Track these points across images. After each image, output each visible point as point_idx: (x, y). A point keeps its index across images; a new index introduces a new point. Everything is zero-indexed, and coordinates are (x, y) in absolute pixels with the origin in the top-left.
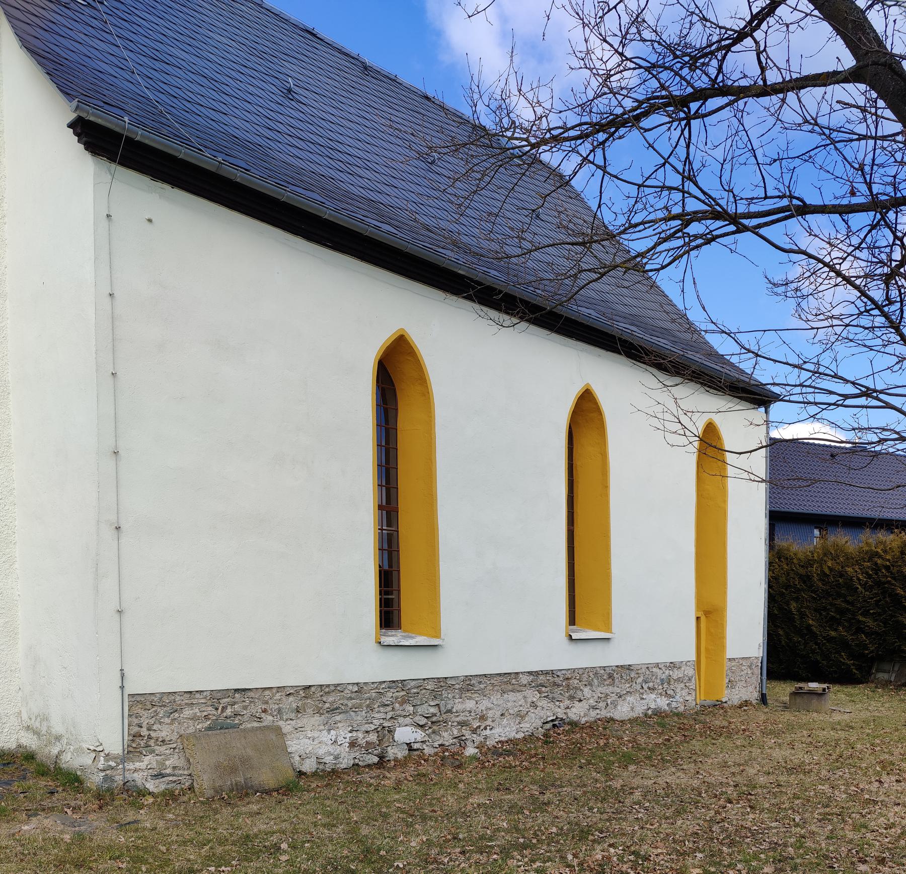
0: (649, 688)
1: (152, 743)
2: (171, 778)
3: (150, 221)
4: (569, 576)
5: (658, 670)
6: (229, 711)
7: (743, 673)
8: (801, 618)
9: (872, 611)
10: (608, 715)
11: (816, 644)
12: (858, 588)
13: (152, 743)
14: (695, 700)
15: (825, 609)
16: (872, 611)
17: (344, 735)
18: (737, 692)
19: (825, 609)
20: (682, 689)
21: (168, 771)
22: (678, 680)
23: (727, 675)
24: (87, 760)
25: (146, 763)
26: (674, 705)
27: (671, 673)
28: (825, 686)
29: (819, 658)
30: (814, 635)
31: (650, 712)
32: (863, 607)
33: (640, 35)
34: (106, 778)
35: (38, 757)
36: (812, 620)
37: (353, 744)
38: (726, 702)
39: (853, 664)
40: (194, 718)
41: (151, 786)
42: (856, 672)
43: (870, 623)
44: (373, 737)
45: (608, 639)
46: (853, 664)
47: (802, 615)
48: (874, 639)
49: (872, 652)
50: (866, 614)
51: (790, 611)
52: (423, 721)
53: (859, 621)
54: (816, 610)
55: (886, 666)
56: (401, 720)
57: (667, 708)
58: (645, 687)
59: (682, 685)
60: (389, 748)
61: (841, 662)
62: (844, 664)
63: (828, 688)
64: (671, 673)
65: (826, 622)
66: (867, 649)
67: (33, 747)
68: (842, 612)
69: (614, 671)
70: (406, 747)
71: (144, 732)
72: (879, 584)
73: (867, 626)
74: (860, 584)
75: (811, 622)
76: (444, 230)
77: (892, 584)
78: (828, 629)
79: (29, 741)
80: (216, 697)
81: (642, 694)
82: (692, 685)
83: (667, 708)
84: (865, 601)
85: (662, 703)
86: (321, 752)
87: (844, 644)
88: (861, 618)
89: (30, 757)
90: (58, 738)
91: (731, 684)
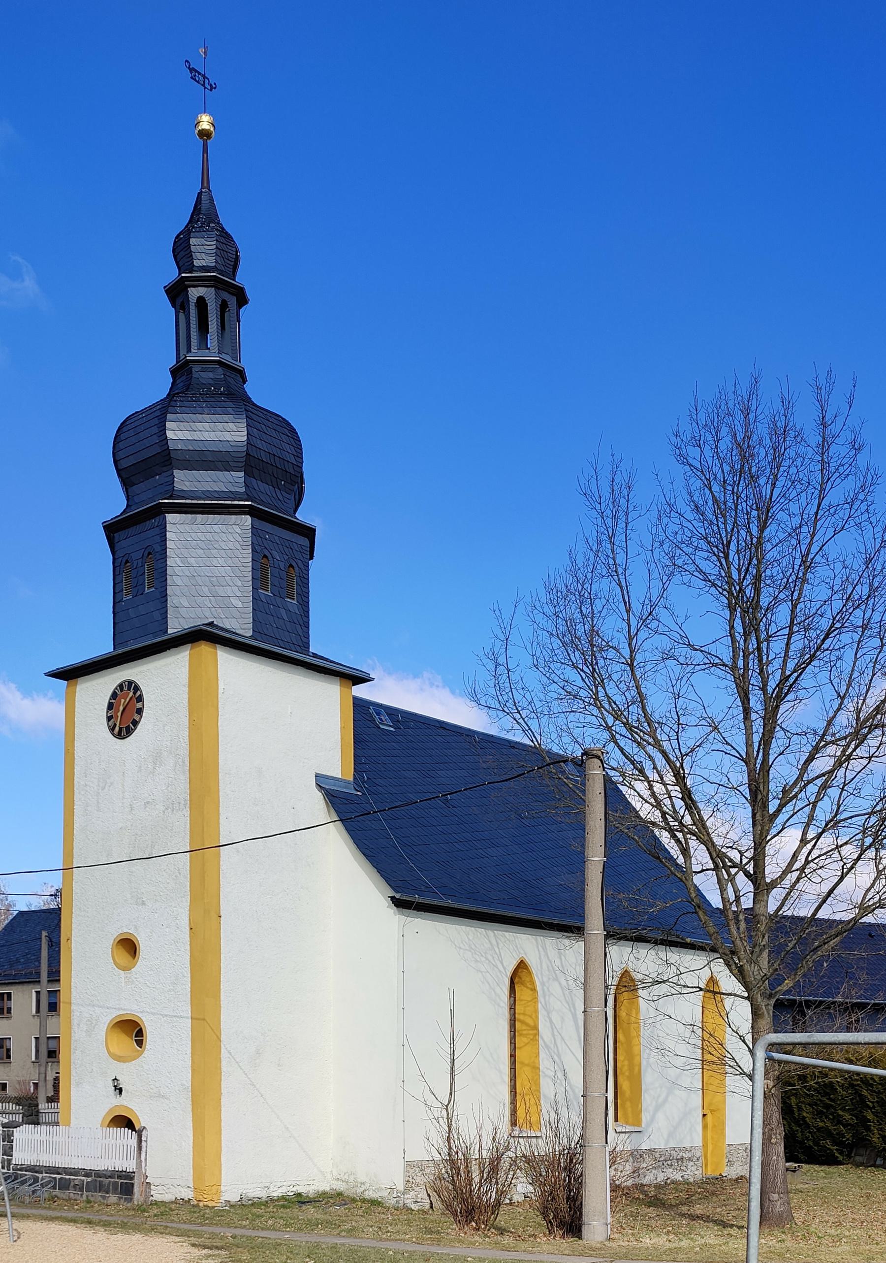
0: (668, 1164)
1: (413, 1185)
2: (420, 1204)
4: (176, 646)
5: (675, 1152)
7: (739, 1155)
8: (799, 1111)
9: (847, 1107)
10: (640, 1182)
11: (810, 1132)
12: (837, 1089)
13: (413, 1185)
14: (702, 1174)
15: (816, 1104)
16: (847, 1107)
18: (735, 1169)
19: (816, 1104)
20: (692, 1166)
21: (419, 1200)
22: (690, 1159)
23: (727, 1157)
24: (385, 1194)
25: (411, 1195)
26: (686, 1177)
27: (684, 1154)
28: (796, 1165)
29: (811, 1143)
30: (808, 1126)
31: (669, 1181)
32: (842, 1104)
33: (667, 789)
34: (397, 1202)
35: (345, 1195)
36: (807, 1113)
38: (726, 1176)
39: (836, 1150)
41: (413, 1206)
42: (839, 1156)
43: (847, 1116)
45: (640, 1131)
46: (836, 1150)
47: (800, 1109)
48: (849, 1129)
49: (848, 1139)
50: (843, 1109)
51: (791, 1105)
53: (839, 1116)
54: (809, 1105)
55: (862, 1151)
57: (681, 1179)
58: (665, 1164)
59: (692, 1163)
60: (514, 1195)
61: (826, 1147)
62: (829, 1149)
63: (799, 1166)
64: (684, 1154)
65: (817, 1115)
66: (845, 1137)
67: (342, 1189)
68: (828, 1107)
69: (644, 1152)
70: (523, 1195)
71: (411, 1180)
72: (852, 1086)
73: (845, 1119)
74: (840, 1086)
75: (805, 1114)
76: (507, 803)
77: (861, 1087)
78: (818, 1120)
79: (340, 1187)
81: (663, 1169)
82: (699, 1163)
83: (681, 1179)
84: (842, 1099)
85: (678, 1176)
87: (828, 1133)
88: (840, 1112)
89: (340, 1194)
90: (363, 1183)
91: (730, 1163)
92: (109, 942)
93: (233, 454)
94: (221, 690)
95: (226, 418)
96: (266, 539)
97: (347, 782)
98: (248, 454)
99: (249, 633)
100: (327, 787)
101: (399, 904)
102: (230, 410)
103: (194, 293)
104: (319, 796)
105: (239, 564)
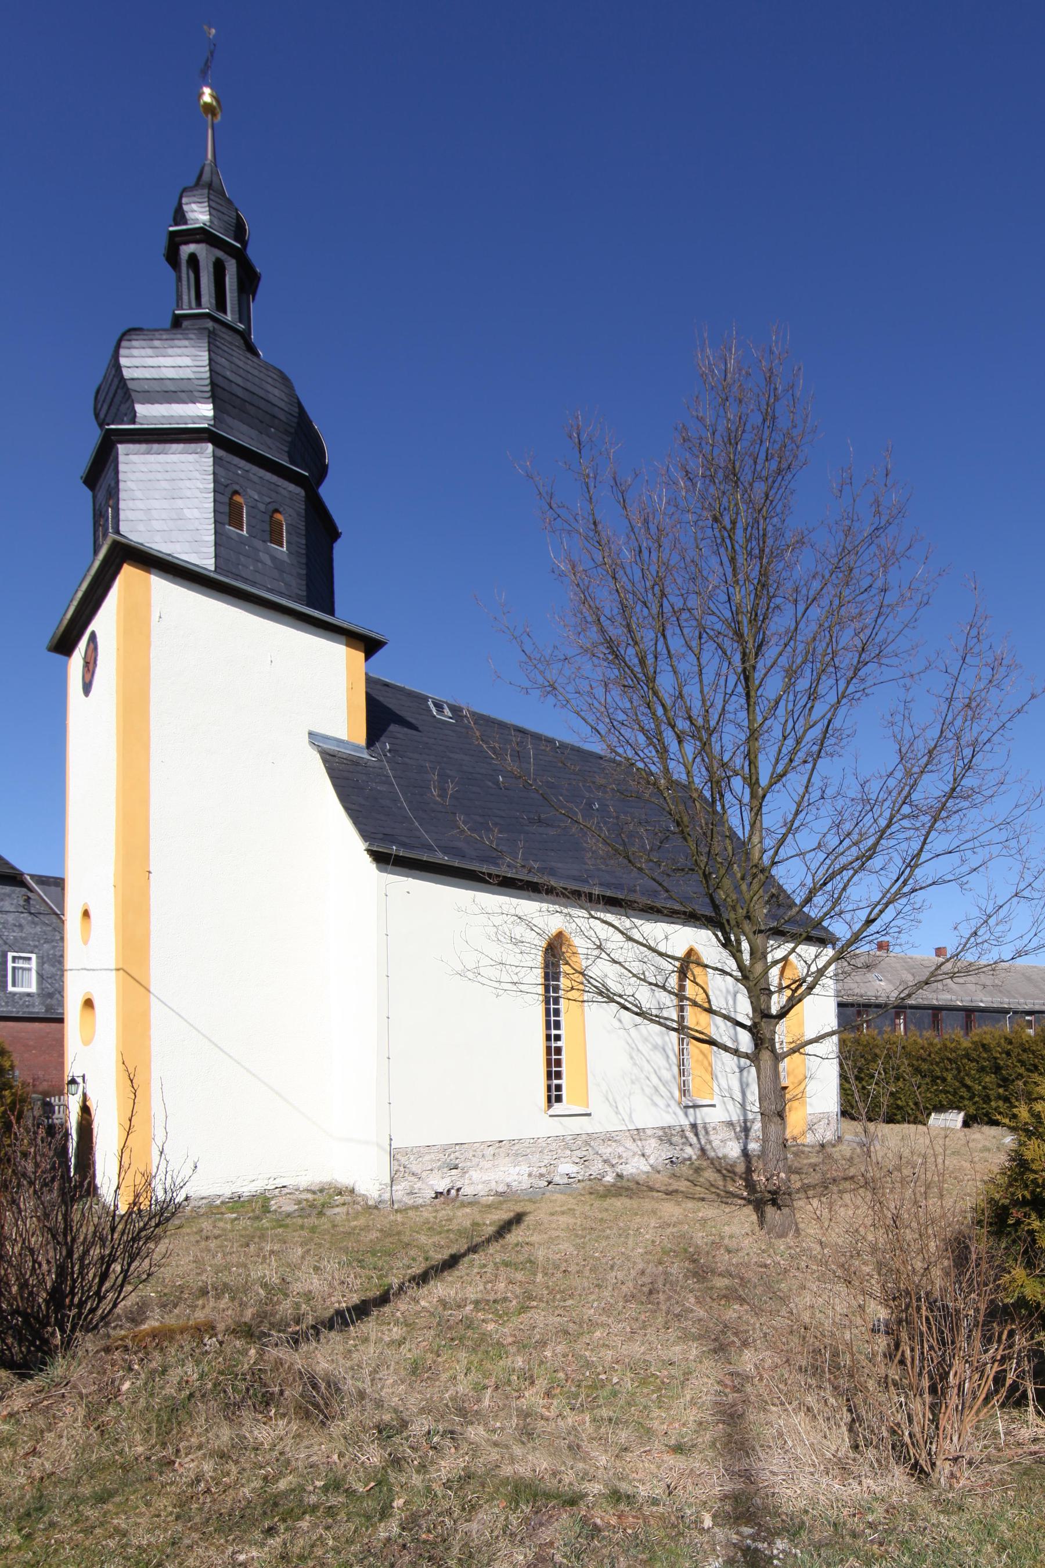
3: (86, 914)
6: (452, 1156)
17: (524, 1169)
37: (530, 1175)
40: (432, 1160)
44: (543, 1170)
52: (578, 1160)
56: (562, 1159)
80: (444, 1149)
86: (508, 1180)
92: (80, 914)
93: (197, 382)
94: (155, 617)
95: (186, 343)
96: (238, 475)
97: (357, 747)
98: (213, 384)
99: (213, 569)
100: (325, 746)
101: (381, 859)
102: (192, 336)
103: (186, 250)
104: (317, 757)
105: (199, 494)
